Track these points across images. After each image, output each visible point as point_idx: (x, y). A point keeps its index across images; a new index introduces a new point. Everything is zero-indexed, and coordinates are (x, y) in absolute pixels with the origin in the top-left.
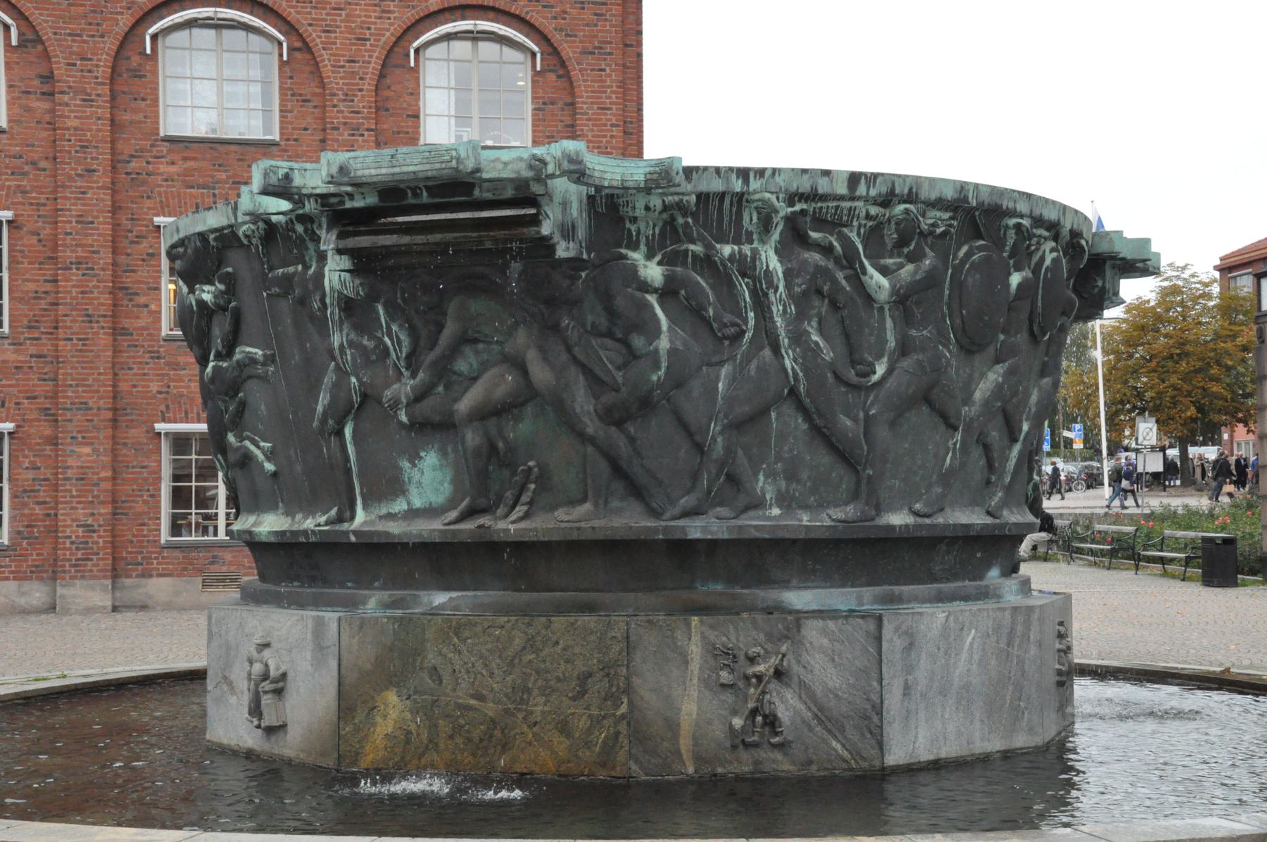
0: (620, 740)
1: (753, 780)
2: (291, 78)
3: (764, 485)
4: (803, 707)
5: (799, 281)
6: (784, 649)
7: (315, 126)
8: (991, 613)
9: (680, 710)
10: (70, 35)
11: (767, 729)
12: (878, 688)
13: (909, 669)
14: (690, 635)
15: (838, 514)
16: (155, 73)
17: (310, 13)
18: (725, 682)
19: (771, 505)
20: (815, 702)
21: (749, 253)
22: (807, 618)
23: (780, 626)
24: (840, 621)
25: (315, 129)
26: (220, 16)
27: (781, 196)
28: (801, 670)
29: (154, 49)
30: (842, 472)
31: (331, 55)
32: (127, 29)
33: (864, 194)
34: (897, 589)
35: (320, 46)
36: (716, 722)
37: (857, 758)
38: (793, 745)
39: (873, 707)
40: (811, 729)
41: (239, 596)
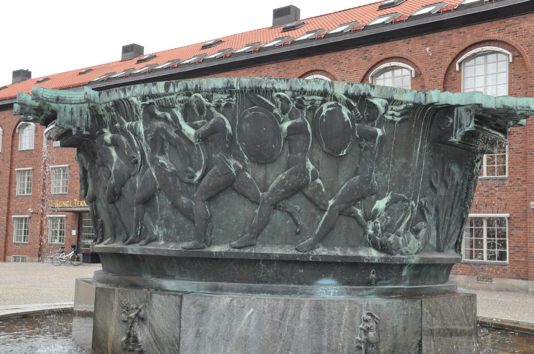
2: (514, 69)
3: (157, 231)
4: (150, 336)
5: (149, 135)
7: (523, 87)
8: (267, 301)
10: (431, 69)
12: (179, 331)
13: (200, 324)
15: (185, 245)
16: (460, 77)
17: (522, 40)
19: (161, 239)
20: (154, 334)
21: (134, 125)
25: (524, 88)
26: (484, 50)
27: (138, 97)
29: (460, 69)
30: (190, 225)
31: (530, 56)
32: (449, 63)
33: (173, 91)
34: (220, 284)
35: (526, 53)
39: (176, 340)
41: (102, 269)
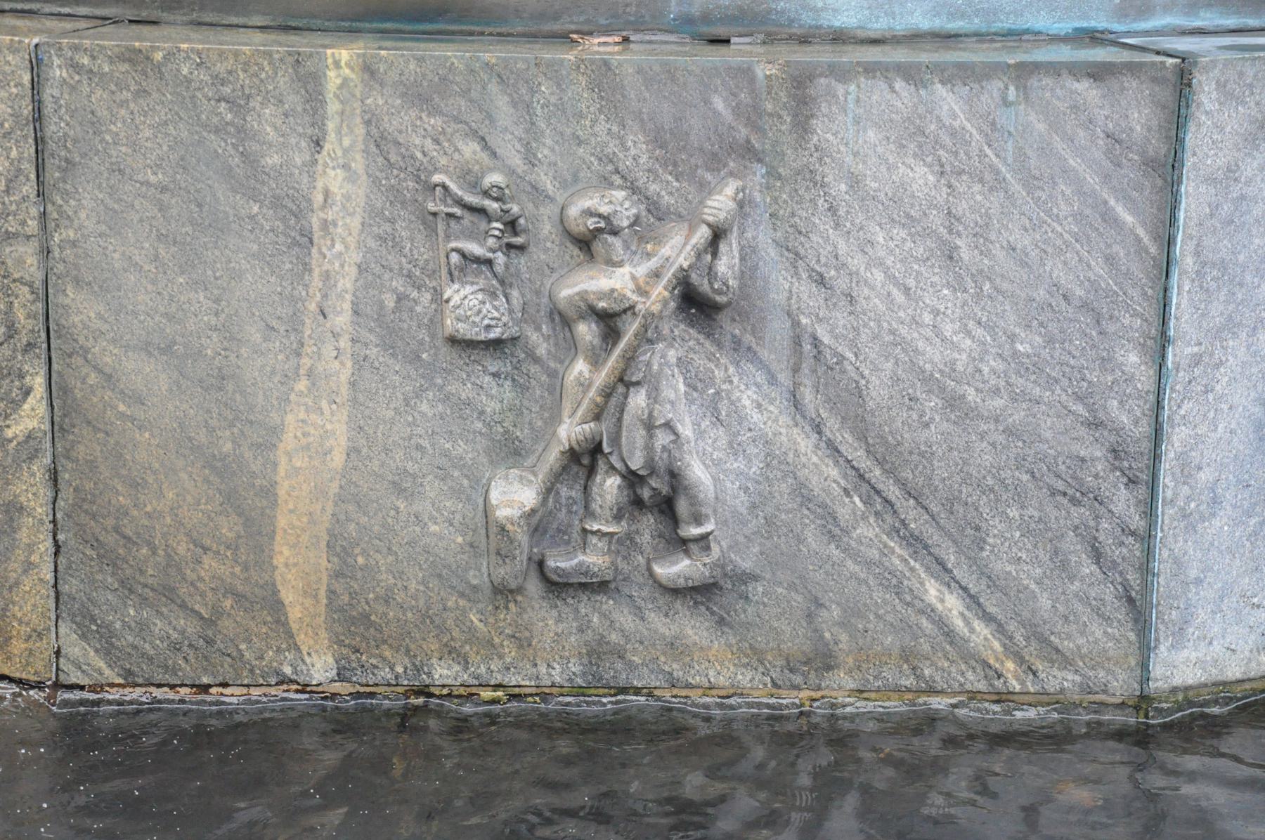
0: (23, 535)
1: (573, 726)
4: (805, 443)
6: (720, 204)
9: (276, 431)
11: (648, 526)
12: (1144, 378)
14: (318, 120)
18: (465, 330)
22: (842, 73)
23: (719, 104)
24: (995, 86)
28: (805, 290)
36: (432, 487)
37: (1031, 652)
38: (757, 590)
40: (834, 531)
